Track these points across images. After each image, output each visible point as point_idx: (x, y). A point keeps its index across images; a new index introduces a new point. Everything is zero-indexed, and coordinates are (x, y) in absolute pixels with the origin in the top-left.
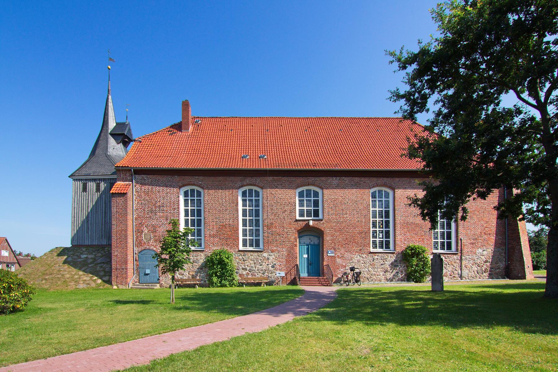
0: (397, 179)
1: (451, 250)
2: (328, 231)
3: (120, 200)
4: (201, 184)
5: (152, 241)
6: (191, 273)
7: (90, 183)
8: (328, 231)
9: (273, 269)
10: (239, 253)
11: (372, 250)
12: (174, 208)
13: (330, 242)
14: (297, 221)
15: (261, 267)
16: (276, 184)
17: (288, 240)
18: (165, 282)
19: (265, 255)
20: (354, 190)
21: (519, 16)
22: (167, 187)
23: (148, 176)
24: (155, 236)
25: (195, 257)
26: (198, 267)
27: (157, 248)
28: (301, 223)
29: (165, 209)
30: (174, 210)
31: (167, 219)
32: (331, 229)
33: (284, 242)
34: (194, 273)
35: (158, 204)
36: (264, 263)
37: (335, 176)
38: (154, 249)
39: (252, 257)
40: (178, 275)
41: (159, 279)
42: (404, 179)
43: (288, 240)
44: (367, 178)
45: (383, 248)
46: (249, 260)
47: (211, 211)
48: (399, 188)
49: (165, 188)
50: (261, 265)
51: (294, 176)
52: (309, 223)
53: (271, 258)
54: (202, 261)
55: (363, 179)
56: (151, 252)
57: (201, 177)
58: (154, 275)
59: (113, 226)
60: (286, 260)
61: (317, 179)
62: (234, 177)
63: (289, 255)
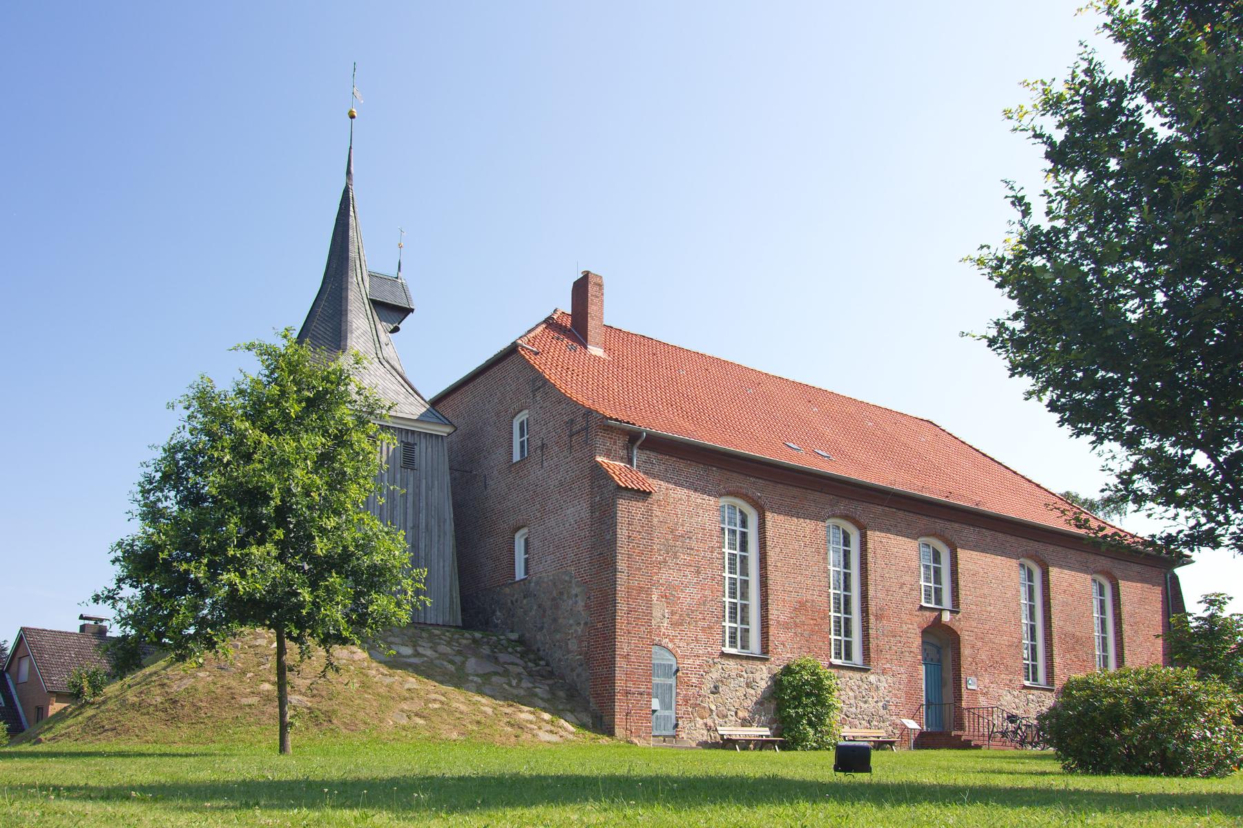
0: (1051, 548)
1: (851, 660)
2: (967, 638)
3: (638, 508)
4: (760, 497)
5: (665, 625)
6: (741, 714)
7: (423, 445)
8: (967, 638)
9: (885, 712)
10: (829, 670)
11: (728, 650)
12: (712, 547)
13: (969, 659)
14: (922, 608)
15: (866, 706)
16: (888, 523)
17: (908, 649)
18: (688, 734)
19: (872, 678)
20: (999, 559)
21: (279, 399)
22: (696, 490)
23: (660, 457)
24: (673, 613)
25: (751, 675)
26: (754, 699)
27: (675, 644)
28: (927, 613)
29: (694, 544)
30: (712, 552)
31: (698, 572)
32: (971, 634)
33: (902, 653)
34: (747, 715)
35: (680, 532)
36: (870, 699)
37: (973, 526)
38: (670, 646)
39: (852, 681)
40: (716, 717)
41: (676, 726)
42: (1059, 549)
43: (908, 649)
44: (1014, 537)
45: (1028, 680)
46: (848, 689)
47: (779, 564)
48: (1054, 565)
49: (694, 495)
50: (866, 702)
51: (927, 516)
52: (940, 615)
53: (883, 685)
54: (763, 685)
55: (1009, 538)
56: (662, 652)
57: (761, 481)
58: (667, 713)
59: (619, 575)
60: (906, 693)
61: (948, 525)
62: (819, 493)
63: (910, 681)
